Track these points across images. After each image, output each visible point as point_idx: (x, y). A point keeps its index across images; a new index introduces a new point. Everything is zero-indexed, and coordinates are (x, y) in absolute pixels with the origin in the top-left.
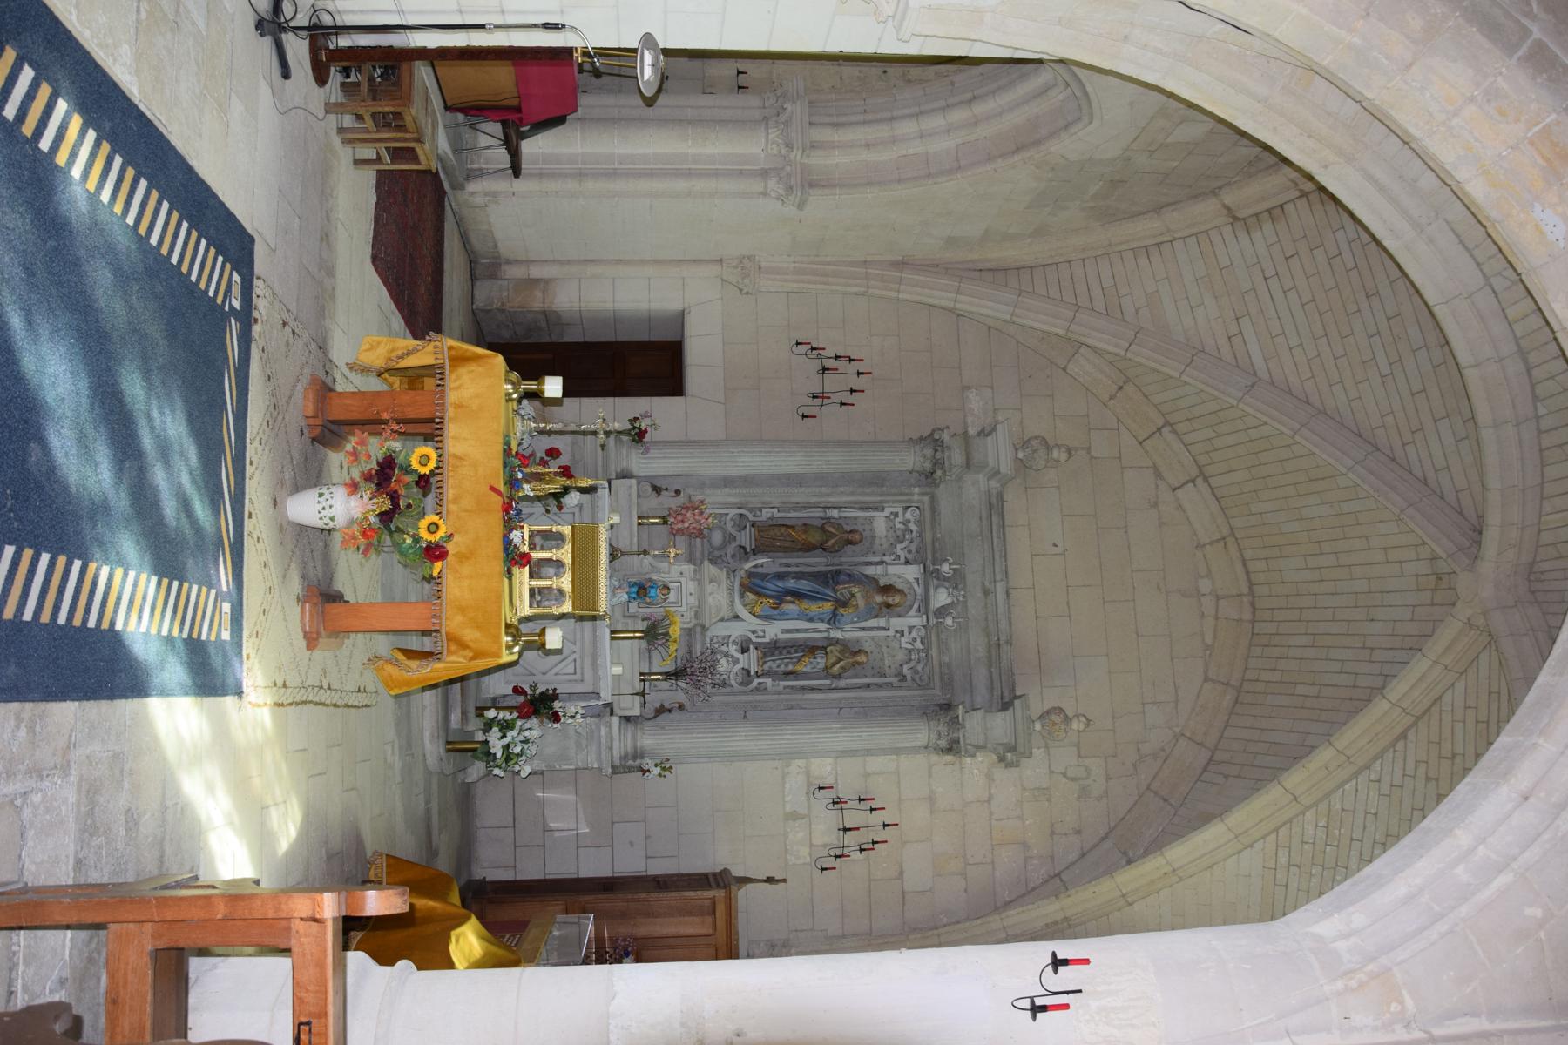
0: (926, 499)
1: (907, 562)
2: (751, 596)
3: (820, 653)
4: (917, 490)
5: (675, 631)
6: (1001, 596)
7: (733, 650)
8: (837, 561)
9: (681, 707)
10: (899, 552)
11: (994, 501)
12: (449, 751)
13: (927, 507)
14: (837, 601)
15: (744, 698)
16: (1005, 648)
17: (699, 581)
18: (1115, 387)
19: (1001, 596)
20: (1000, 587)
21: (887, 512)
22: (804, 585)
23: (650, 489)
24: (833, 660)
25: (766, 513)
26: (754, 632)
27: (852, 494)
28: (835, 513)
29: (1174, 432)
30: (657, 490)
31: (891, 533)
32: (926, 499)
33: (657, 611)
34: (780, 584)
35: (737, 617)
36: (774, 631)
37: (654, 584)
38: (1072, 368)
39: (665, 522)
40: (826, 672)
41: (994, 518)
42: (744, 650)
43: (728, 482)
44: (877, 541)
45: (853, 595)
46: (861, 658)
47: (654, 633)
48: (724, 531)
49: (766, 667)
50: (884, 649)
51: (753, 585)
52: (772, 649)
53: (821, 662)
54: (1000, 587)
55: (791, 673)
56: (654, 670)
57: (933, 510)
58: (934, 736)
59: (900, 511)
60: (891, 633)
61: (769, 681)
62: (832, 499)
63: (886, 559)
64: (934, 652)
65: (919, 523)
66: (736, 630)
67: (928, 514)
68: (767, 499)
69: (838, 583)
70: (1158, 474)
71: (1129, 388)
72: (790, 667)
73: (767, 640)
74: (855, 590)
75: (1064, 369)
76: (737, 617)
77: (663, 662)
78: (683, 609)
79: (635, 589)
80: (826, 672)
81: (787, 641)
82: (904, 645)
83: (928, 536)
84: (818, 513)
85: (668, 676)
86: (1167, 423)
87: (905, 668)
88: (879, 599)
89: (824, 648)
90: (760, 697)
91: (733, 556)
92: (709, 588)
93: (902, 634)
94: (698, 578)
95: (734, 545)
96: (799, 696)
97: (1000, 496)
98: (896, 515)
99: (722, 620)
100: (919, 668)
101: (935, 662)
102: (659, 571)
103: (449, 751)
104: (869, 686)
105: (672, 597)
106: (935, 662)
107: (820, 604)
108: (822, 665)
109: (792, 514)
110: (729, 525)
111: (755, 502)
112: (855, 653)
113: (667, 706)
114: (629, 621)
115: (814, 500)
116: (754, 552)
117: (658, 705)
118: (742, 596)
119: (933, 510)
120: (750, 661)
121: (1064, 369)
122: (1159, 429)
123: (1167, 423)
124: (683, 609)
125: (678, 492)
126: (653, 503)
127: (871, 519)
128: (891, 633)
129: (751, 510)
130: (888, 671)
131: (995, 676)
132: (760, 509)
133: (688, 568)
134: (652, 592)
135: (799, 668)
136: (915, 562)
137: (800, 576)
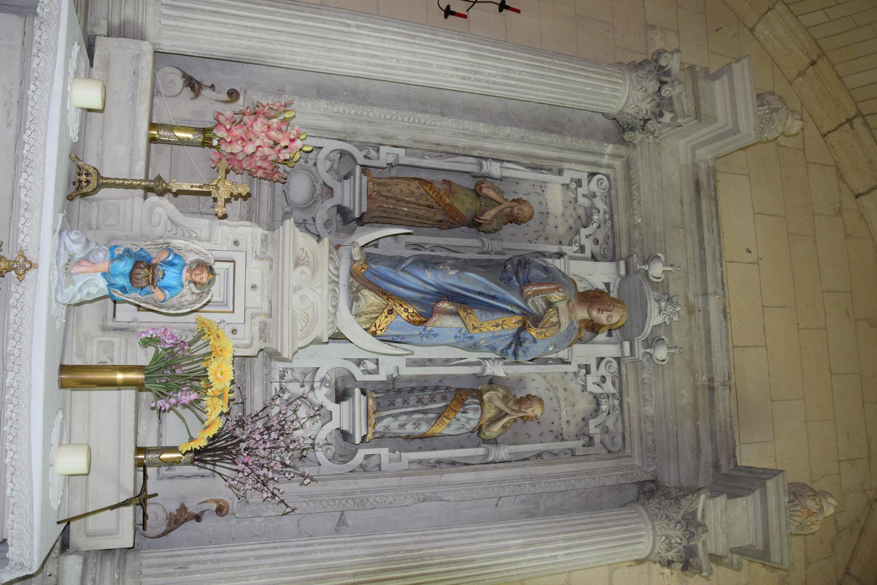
0: (618, 163)
1: (594, 258)
2: (370, 299)
3: (472, 403)
4: (610, 148)
5: (221, 373)
6: (715, 317)
7: (322, 396)
8: (496, 245)
9: (221, 510)
10: (584, 241)
11: (703, 179)
12: (63, 385)
13: (620, 176)
14: (526, 313)
15: (340, 485)
16: (722, 394)
17: (272, 262)
18: (807, 61)
19: (715, 317)
20: (714, 303)
21: (566, 178)
22: (474, 282)
23: (180, 82)
24: (490, 413)
25: (386, 155)
26: (359, 362)
27: (521, 141)
28: (494, 169)
29: (866, 124)
30: (193, 85)
31: (570, 211)
32: (618, 163)
33: (181, 327)
34: (429, 276)
35: (338, 337)
36: (393, 364)
37: (174, 260)
38: (762, 30)
39: (206, 143)
40: (478, 436)
41: (704, 203)
42: (341, 396)
43: (325, 89)
44: (551, 221)
45: (550, 304)
46: (534, 410)
47: (170, 375)
48: (314, 178)
49: (380, 427)
50: (561, 394)
51: (368, 276)
52: (391, 394)
53: (471, 417)
54: (714, 303)
55: (422, 437)
56: (168, 442)
57: (629, 181)
58: (661, 545)
59: (584, 177)
60: (572, 368)
61: (384, 452)
62: (488, 145)
63: (566, 249)
64: (631, 399)
65: (609, 198)
66: (331, 360)
67: (621, 185)
68: (388, 130)
69: (528, 282)
70: (841, 177)
71: (822, 64)
72: (424, 429)
73: (382, 377)
74: (555, 297)
75: (752, 30)
76: (338, 337)
77: (182, 432)
78: (236, 318)
79: (125, 266)
80: (478, 436)
81: (410, 379)
82: (591, 388)
83: (621, 220)
84: (468, 164)
85: (199, 456)
86: (859, 114)
87: (592, 423)
88: (582, 314)
89: (479, 394)
90: (367, 483)
91: (327, 224)
92: (294, 276)
93: (587, 369)
94: (269, 254)
95: (330, 203)
96: (435, 478)
97: (712, 173)
98: (579, 183)
99: (317, 341)
100: (610, 423)
101: (634, 414)
102: (189, 236)
103: (63, 385)
104: (539, 455)
105: (217, 292)
106: (634, 414)
107: (499, 318)
108: (474, 424)
109: (428, 162)
110: (323, 167)
111: (369, 134)
112: (520, 401)
113: (193, 508)
114: (117, 340)
115: (463, 142)
116: (361, 221)
117: (173, 508)
118: (354, 298)
119: (629, 181)
120: (351, 415)
121: (752, 30)
122: (849, 121)
123: (859, 114)
124: (236, 318)
125: (233, 95)
126: (182, 109)
127: (543, 184)
128: (572, 368)
129: (361, 146)
130: (566, 430)
131: (704, 436)
132: (377, 147)
133: (250, 233)
134: (171, 276)
135: (438, 429)
136: (604, 258)
137: (464, 266)
